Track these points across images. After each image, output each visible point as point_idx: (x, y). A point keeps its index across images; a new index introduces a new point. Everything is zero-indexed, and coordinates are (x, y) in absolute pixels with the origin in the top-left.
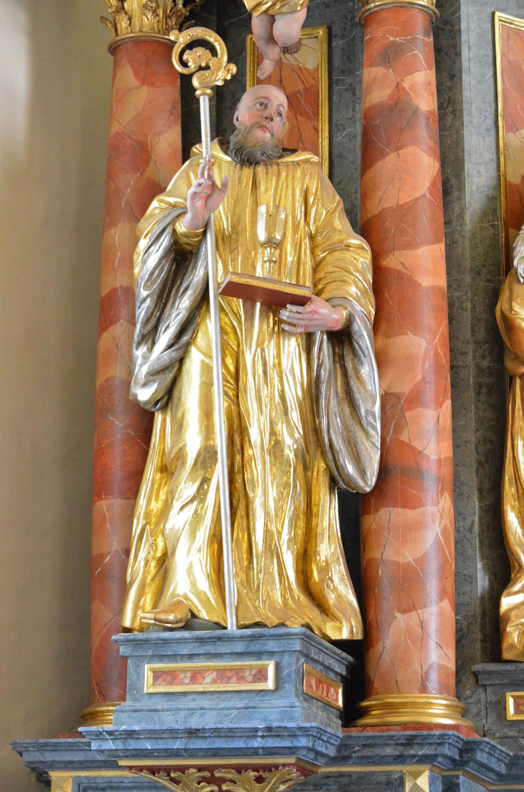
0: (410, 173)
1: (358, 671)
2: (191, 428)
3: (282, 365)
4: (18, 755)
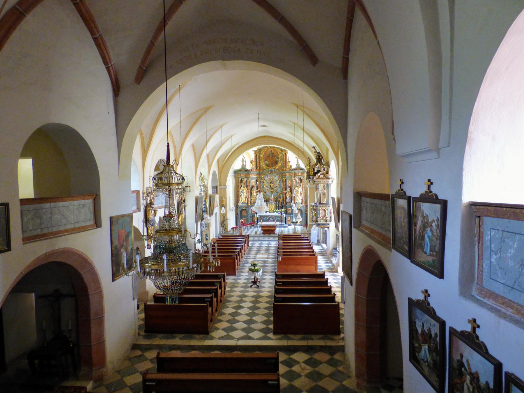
0: (249, 187)
1: (247, 204)
2: (242, 196)
3: (245, 194)
4: (132, 298)
